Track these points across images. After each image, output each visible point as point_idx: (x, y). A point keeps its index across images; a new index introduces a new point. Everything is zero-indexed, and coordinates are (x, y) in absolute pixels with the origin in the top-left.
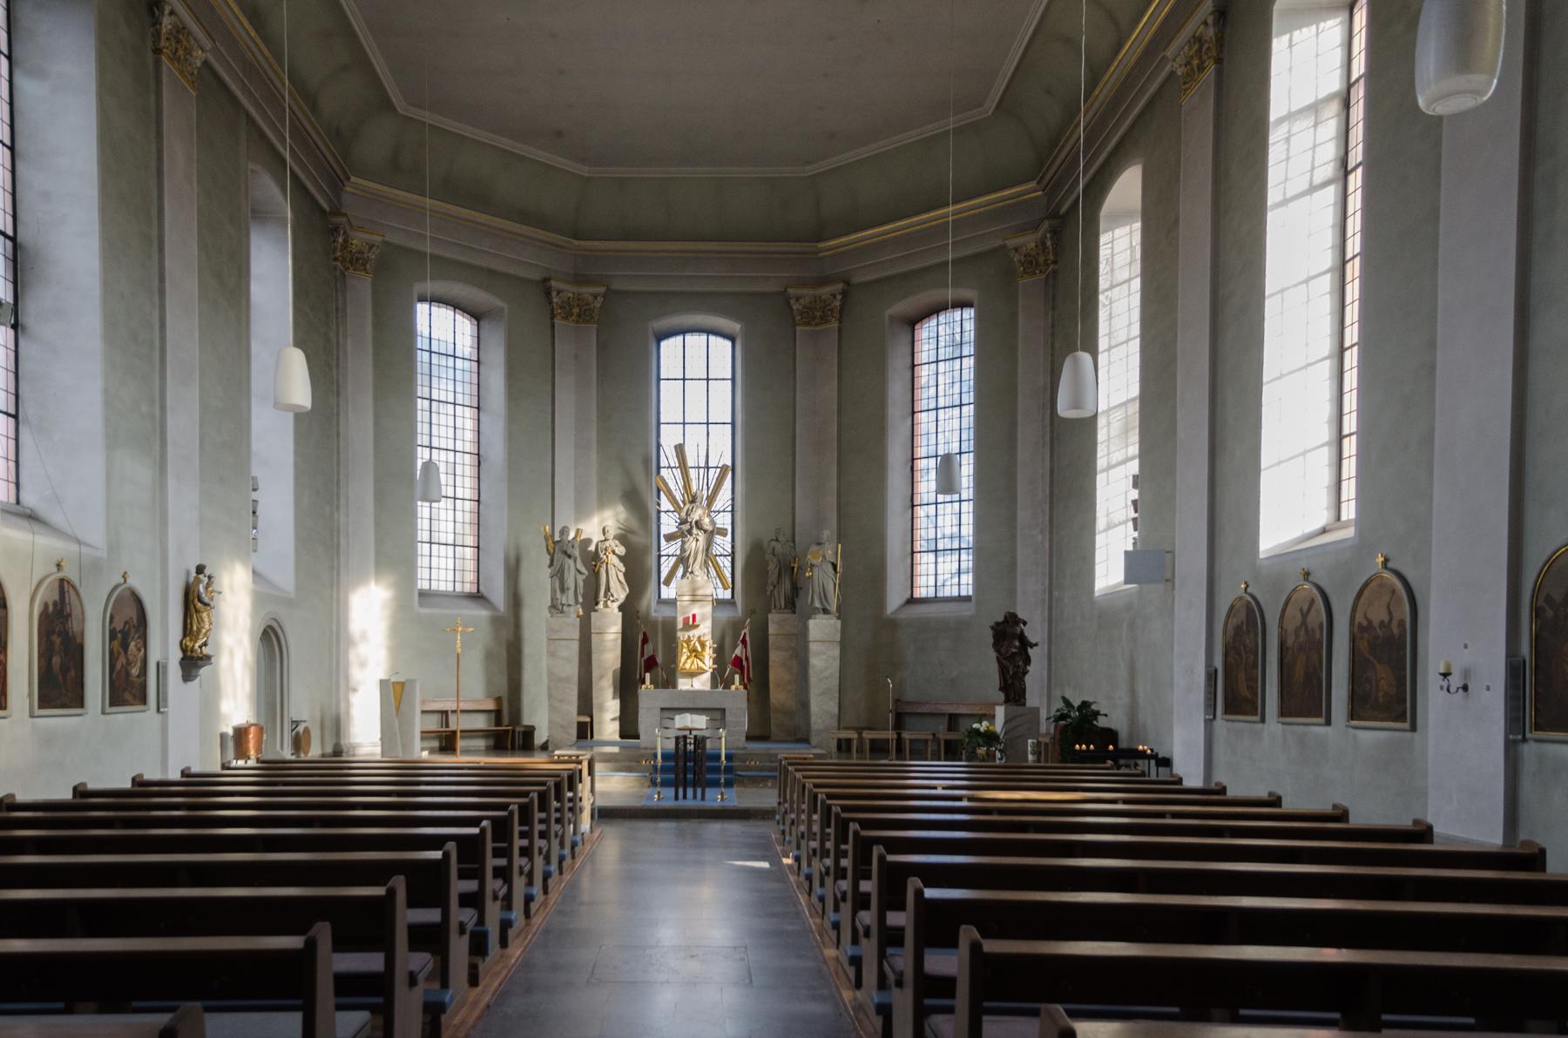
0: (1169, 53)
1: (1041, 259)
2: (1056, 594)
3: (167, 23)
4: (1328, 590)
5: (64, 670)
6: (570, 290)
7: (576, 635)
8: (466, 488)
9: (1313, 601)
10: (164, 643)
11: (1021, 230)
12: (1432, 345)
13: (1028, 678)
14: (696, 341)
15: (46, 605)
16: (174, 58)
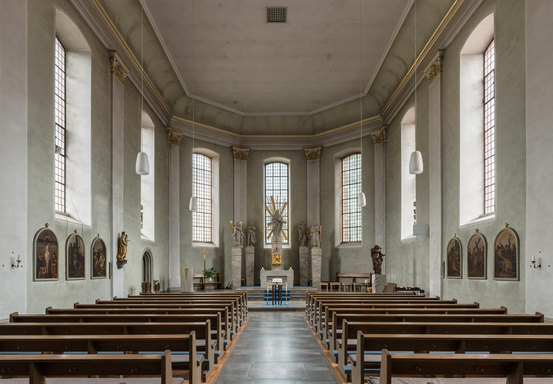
0: (425, 71)
1: (382, 138)
2: (388, 240)
3: (115, 63)
4: (485, 236)
5: (78, 265)
6: (239, 150)
7: (240, 254)
8: (207, 209)
9: (480, 239)
10: (111, 256)
11: (375, 130)
12: (524, 153)
13: (382, 266)
14: (277, 165)
15: (71, 244)
16: (117, 75)
